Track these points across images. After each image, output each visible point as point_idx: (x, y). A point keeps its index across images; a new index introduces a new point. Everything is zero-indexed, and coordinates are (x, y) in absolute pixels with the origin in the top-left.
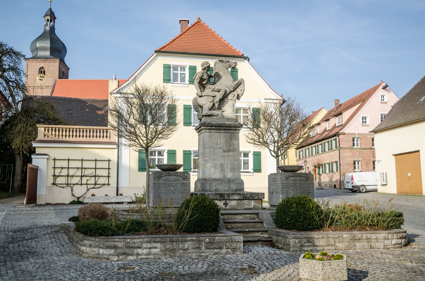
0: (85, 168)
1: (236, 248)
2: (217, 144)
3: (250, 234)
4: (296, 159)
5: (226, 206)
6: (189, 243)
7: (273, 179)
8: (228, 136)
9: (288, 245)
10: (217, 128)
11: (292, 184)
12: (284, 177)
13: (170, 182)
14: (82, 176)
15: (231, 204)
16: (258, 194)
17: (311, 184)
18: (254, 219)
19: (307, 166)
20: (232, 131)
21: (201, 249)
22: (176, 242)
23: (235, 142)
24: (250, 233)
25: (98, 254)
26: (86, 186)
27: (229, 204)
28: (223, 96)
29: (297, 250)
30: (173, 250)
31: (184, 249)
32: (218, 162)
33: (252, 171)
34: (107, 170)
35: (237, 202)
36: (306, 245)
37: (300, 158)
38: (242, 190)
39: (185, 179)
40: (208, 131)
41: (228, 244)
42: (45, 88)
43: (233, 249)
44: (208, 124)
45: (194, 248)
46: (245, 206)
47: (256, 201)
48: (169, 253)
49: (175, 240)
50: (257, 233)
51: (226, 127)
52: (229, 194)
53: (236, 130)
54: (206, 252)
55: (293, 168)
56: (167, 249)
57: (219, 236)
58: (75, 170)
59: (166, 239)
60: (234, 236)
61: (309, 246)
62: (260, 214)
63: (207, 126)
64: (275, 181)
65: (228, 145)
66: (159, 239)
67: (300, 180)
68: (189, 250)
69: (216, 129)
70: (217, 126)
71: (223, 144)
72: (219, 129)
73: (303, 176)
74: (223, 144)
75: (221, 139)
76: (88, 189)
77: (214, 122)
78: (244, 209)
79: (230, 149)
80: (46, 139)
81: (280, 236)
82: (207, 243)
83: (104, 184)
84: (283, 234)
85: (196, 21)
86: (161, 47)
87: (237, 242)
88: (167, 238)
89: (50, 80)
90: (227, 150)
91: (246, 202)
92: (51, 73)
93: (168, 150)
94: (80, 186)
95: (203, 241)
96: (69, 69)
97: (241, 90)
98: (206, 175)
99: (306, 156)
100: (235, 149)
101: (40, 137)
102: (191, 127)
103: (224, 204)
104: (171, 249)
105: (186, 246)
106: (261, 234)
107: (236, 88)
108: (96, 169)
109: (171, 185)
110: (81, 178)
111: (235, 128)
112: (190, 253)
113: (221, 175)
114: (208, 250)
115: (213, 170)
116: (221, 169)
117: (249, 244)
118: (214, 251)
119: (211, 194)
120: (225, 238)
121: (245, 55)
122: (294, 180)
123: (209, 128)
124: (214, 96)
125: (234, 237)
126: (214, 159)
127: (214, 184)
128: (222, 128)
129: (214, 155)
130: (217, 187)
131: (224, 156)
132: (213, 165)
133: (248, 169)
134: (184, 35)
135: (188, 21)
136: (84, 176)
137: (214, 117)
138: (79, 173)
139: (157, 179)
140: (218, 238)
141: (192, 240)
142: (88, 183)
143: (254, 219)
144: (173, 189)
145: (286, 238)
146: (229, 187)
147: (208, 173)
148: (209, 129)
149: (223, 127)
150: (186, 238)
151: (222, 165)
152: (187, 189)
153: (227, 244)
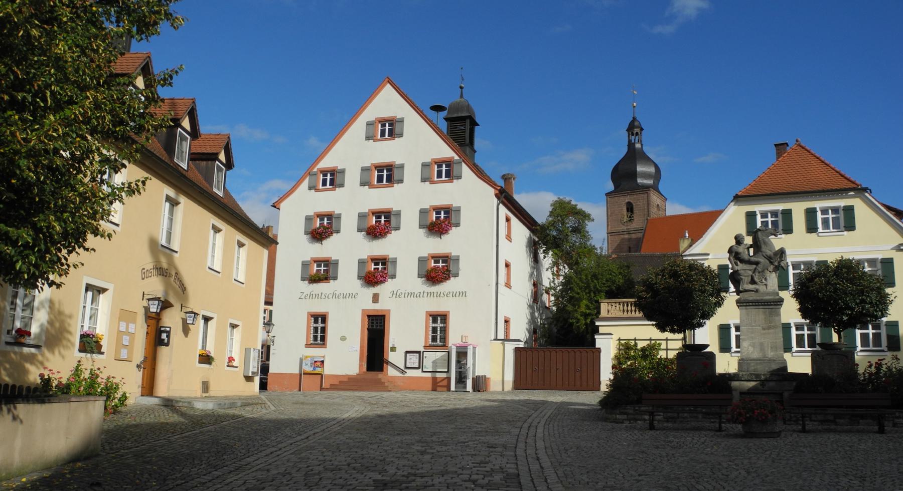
10: (754, 304)
23: (776, 318)
25: (616, 419)
33: (886, 349)
34: (668, 351)
53: (778, 305)
69: (753, 305)
80: (610, 315)
101: (604, 313)
108: (668, 351)
113: (761, 354)
115: (751, 349)
121: (864, 186)
131: (764, 334)
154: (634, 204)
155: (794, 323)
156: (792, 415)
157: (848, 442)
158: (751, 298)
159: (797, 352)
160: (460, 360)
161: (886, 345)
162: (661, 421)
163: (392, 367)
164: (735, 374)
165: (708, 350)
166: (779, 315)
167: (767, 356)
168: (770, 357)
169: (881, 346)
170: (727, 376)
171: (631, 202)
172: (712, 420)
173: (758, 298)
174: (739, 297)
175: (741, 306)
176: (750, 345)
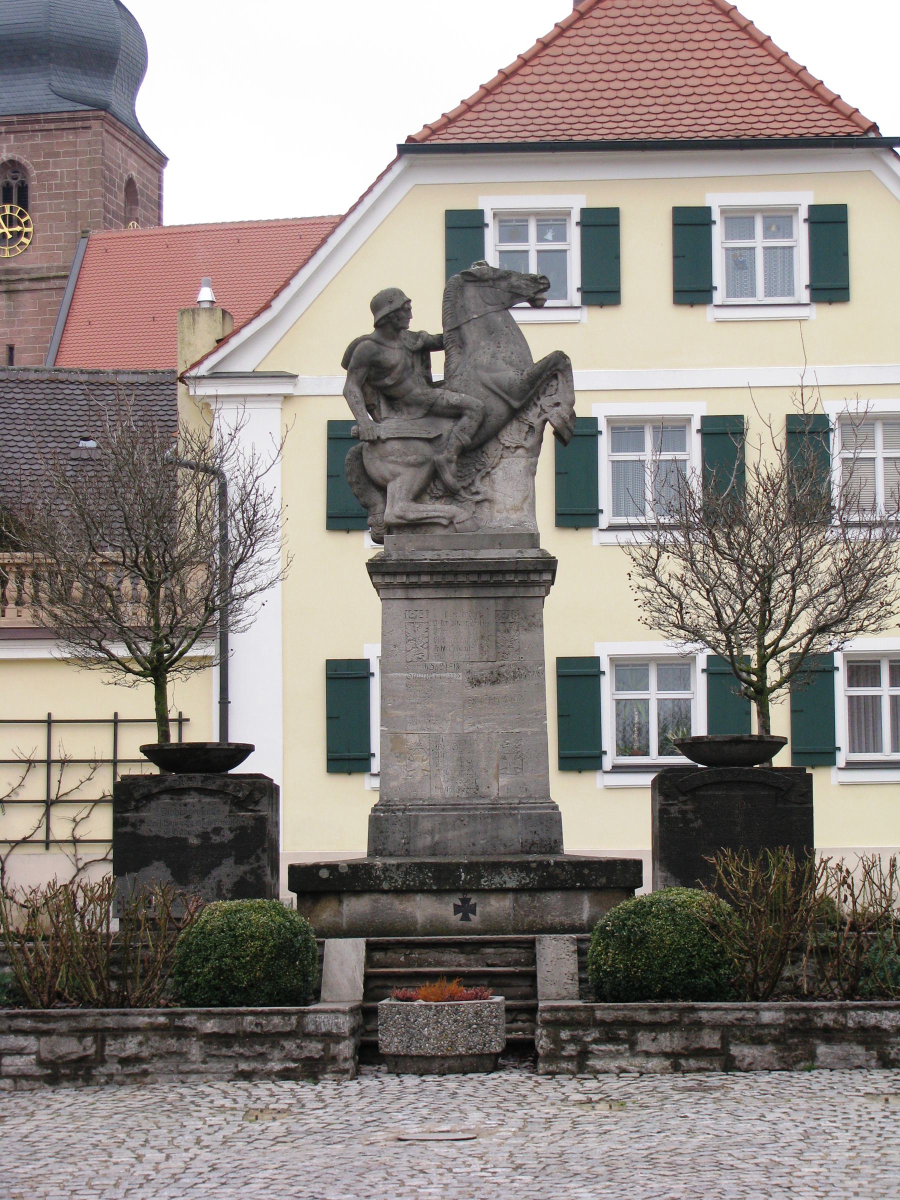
0: (64, 762)
2: (443, 648)
5: (466, 918)
10: (439, 579)
14: (49, 804)
15: (488, 909)
20: (510, 592)
21: (187, 1061)
23: (524, 637)
26: (69, 849)
27: (478, 909)
32: (445, 729)
38: (555, 845)
42: (27, 285)
44: (400, 563)
51: (479, 573)
53: (525, 584)
58: (84, 772)
63: (395, 574)
65: (492, 653)
69: (437, 585)
70: (439, 573)
71: (468, 649)
74: (468, 649)
76: (81, 865)
79: (503, 670)
86: (433, 118)
89: (57, 239)
91: (554, 899)
92: (58, 196)
94: (41, 849)
96: (162, 160)
98: (394, 784)
102: (594, 532)
103: (457, 909)
110: (47, 814)
116: (460, 759)
119: (399, 866)
123: (404, 579)
124: (431, 436)
128: (461, 578)
130: (437, 837)
131: (474, 700)
132: (425, 741)
134: (558, 51)
136: (57, 801)
137: (440, 531)
138: (35, 789)
142: (81, 833)
143: (517, 963)
151: (464, 743)
154: (34, 173)
156: (565, 1035)
157: (762, 1146)
158: (428, 556)
159: (851, 766)
160: (375, 347)
162: (27, 1077)
164: (355, 868)
165: (242, 768)
166: (535, 624)
167: (483, 790)
168: (494, 791)
170: (324, 874)
171: (24, 161)
172: (244, 1066)
173: (457, 555)
174: (380, 548)
175: (388, 586)
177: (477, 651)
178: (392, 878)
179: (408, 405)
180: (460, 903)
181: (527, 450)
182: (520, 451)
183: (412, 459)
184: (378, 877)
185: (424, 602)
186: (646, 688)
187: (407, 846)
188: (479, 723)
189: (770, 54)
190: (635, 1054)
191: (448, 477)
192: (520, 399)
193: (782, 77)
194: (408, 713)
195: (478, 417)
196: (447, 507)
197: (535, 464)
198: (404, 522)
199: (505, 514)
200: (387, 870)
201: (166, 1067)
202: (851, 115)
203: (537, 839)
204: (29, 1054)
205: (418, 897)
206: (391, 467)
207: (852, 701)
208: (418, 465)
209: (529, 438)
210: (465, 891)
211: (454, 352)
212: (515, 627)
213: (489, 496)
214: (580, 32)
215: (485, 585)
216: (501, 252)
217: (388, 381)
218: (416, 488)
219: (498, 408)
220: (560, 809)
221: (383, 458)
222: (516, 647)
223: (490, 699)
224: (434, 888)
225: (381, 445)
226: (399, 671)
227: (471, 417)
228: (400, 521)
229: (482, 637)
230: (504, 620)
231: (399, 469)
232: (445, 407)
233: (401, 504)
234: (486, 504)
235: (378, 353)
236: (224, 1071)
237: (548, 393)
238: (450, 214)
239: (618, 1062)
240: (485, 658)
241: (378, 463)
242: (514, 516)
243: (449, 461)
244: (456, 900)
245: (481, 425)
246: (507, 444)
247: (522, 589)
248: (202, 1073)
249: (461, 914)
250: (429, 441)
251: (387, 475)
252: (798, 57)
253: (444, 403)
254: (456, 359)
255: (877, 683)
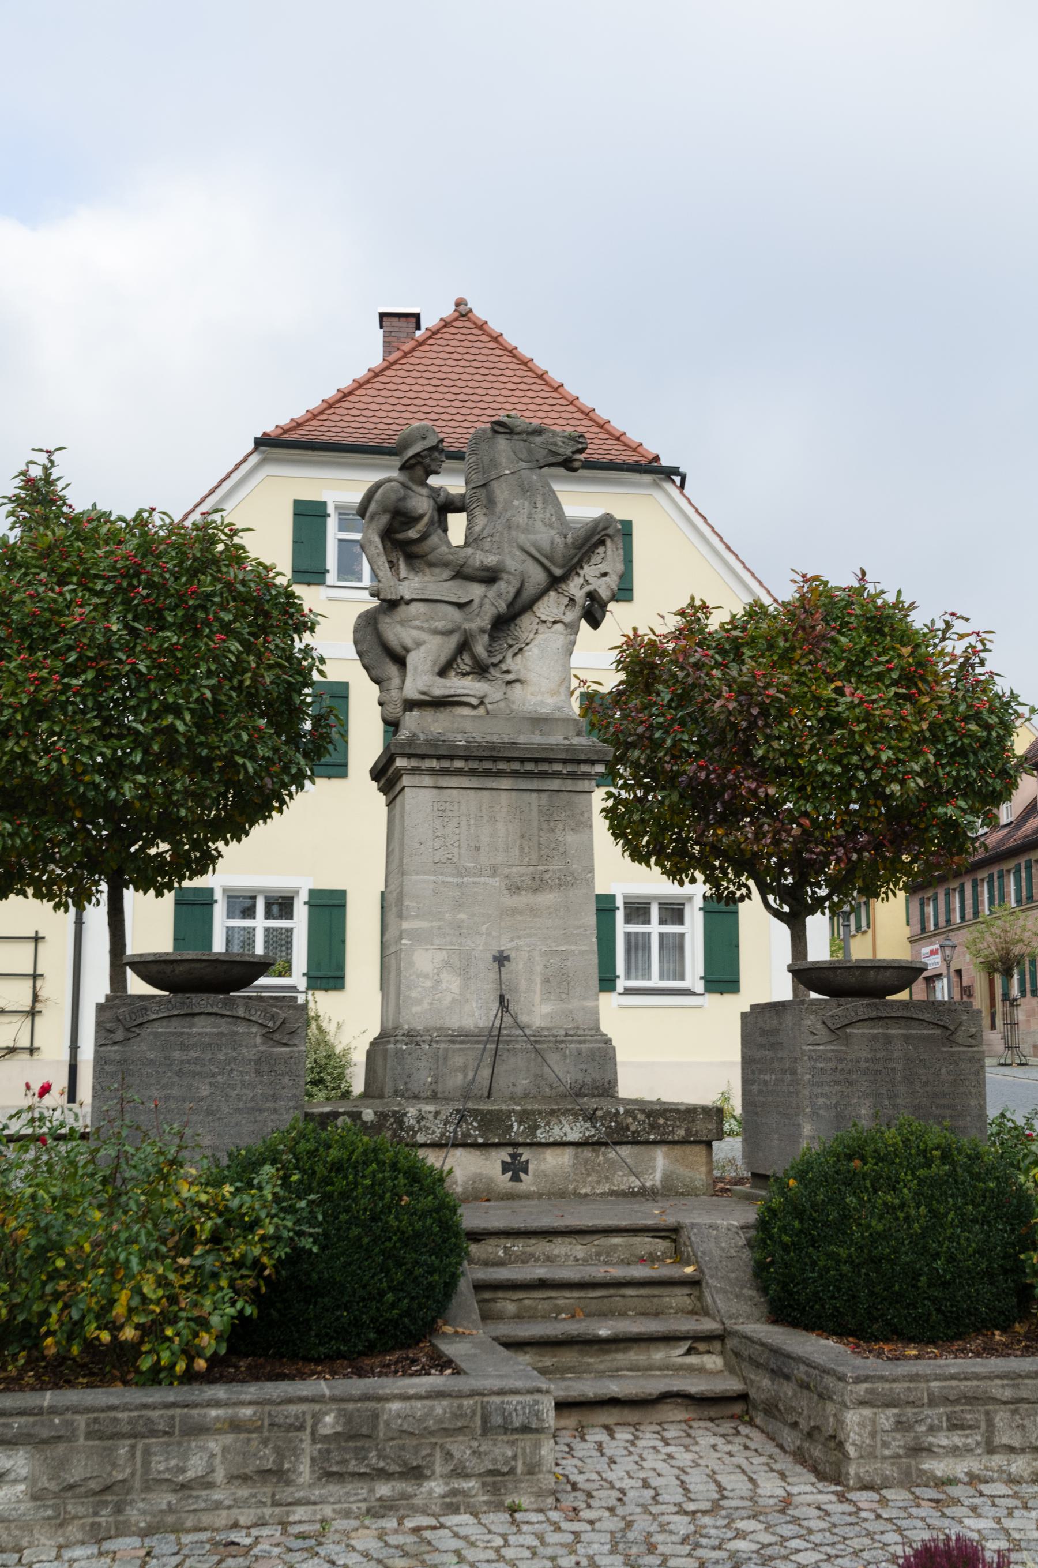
1: (512, 1471)
2: (477, 848)
3: (620, 1356)
4: (907, 932)
6: (212, 1445)
7: (764, 1033)
8: (535, 809)
9: (832, 1444)
10: (475, 765)
11: (867, 1060)
12: (820, 1026)
13: (193, 1054)
15: (543, 1167)
16: (689, 1113)
17: (971, 1060)
18: (651, 1259)
19: (954, 966)
20: (555, 784)
21: (288, 1483)
22: (134, 1436)
23: (570, 838)
24: (625, 1350)
27: (531, 1167)
28: (510, 605)
29: (886, 1478)
30: (107, 1489)
31: (183, 1486)
33: (699, 987)
35: (576, 1157)
36: (944, 1442)
37: (923, 929)
38: (607, 1089)
39: (277, 1036)
40: (427, 780)
41: (461, 1448)
43: (489, 1479)
44: (433, 743)
45: (245, 1478)
46: (616, 1179)
47: (677, 1150)
48: (81, 1510)
49: (126, 1428)
50: (661, 1345)
51: (522, 760)
52: (533, 1112)
53: (573, 776)
54: (322, 1502)
55: (872, 973)
56: (71, 1487)
57: (405, 1398)
59: (69, 1423)
60: (501, 1392)
61: (955, 1451)
62: (684, 1233)
63: (423, 757)
64: (774, 1046)
65: (534, 856)
66: (23, 1420)
67: (907, 1038)
68: (210, 1485)
69: (473, 773)
72: (487, 773)
73: (926, 1016)
74: (507, 850)
75: (500, 825)
77: (459, 737)
78: (612, 1193)
79: (546, 876)
81: (787, 1377)
82: (326, 1438)
83: (12, 1050)
84: (803, 1368)
85: (448, 311)
87: (516, 1430)
88: (76, 1410)
90: (527, 880)
93: (312, 892)
95: (301, 1428)
97: (605, 575)
98: (416, 1009)
99: (948, 921)
100: (572, 874)
103: (506, 1167)
104: (93, 1485)
105: (195, 1467)
106: (689, 1352)
107: (580, 564)
109: (198, 1069)
111: (570, 768)
112: (218, 1505)
114: (334, 1489)
115: (452, 984)
117: (609, 1416)
118: (372, 1491)
120: (440, 1407)
121: (665, 462)
122: (875, 1038)
123: (434, 764)
124: (463, 600)
125: (497, 1399)
126: (459, 929)
127: (458, 1060)
128: (502, 766)
129: (459, 905)
131: (514, 911)
133: (682, 978)
135: (417, 317)
137: (466, 711)
139: (119, 1035)
140: (395, 1406)
141: (235, 1426)
143: (651, 1259)
144: (205, 1091)
145: (821, 1396)
146: (536, 1076)
147: (427, 1001)
148: (432, 772)
149: (509, 760)
150: (195, 1412)
152: (285, 1093)
153: (454, 1448)
155: (225, 890)
159: (628, 992)
160: (402, 492)
161: (700, 971)
163: (124, 946)
169: (682, 978)
176: (447, 965)
177: (517, 853)
178: (428, 1128)
179: (431, 565)
180: (509, 1160)
181: (565, 625)
182: (559, 627)
183: (440, 625)
184: (411, 1128)
185: (455, 792)
186: (267, 930)
187: (434, 1087)
188: (519, 938)
189: (563, 397)
190: (991, 1450)
191: (480, 649)
192: (563, 566)
193: (575, 415)
194: (436, 924)
195: (516, 584)
196: (478, 685)
197: (574, 643)
198: (428, 698)
199: (539, 698)
200: (423, 1118)
201: (254, 1496)
202: (636, 448)
203: (588, 1080)
204: (15, 1481)
205: (459, 1152)
206: (415, 633)
207: (628, 935)
208: (448, 633)
209: (568, 613)
210: (515, 1145)
211: (479, 512)
212: (560, 826)
213: (521, 677)
214: (405, 367)
215: (528, 775)
216: (340, 540)
217: (413, 534)
218: (443, 660)
219: (537, 577)
220: (614, 1043)
221: (403, 623)
222: (562, 850)
223: (532, 910)
224: (480, 1140)
225: (403, 608)
226: (425, 874)
227: (508, 582)
228: (423, 697)
229: (523, 836)
230: (548, 817)
231: (424, 636)
232: (477, 569)
233: (425, 678)
234: (518, 685)
235: (403, 499)
236: (352, 1499)
237: (593, 561)
238: (297, 503)
239: (965, 1464)
240: (526, 861)
241: (399, 628)
242: (550, 701)
243: (482, 631)
244: (504, 1155)
245: (518, 593)
246: (544, 618)
247: (569, 782)
248: (315, 1503)
249: (510, 1174)
250: (460, 606)
251: (409, 643)
252: (587, 401)
253: (477, 564)
254: (481, 521)
255: (647, 921)
